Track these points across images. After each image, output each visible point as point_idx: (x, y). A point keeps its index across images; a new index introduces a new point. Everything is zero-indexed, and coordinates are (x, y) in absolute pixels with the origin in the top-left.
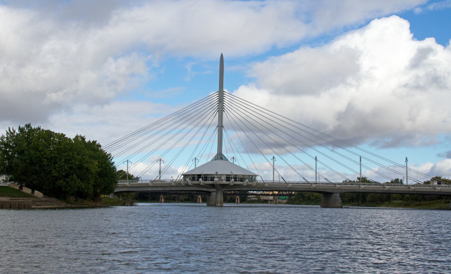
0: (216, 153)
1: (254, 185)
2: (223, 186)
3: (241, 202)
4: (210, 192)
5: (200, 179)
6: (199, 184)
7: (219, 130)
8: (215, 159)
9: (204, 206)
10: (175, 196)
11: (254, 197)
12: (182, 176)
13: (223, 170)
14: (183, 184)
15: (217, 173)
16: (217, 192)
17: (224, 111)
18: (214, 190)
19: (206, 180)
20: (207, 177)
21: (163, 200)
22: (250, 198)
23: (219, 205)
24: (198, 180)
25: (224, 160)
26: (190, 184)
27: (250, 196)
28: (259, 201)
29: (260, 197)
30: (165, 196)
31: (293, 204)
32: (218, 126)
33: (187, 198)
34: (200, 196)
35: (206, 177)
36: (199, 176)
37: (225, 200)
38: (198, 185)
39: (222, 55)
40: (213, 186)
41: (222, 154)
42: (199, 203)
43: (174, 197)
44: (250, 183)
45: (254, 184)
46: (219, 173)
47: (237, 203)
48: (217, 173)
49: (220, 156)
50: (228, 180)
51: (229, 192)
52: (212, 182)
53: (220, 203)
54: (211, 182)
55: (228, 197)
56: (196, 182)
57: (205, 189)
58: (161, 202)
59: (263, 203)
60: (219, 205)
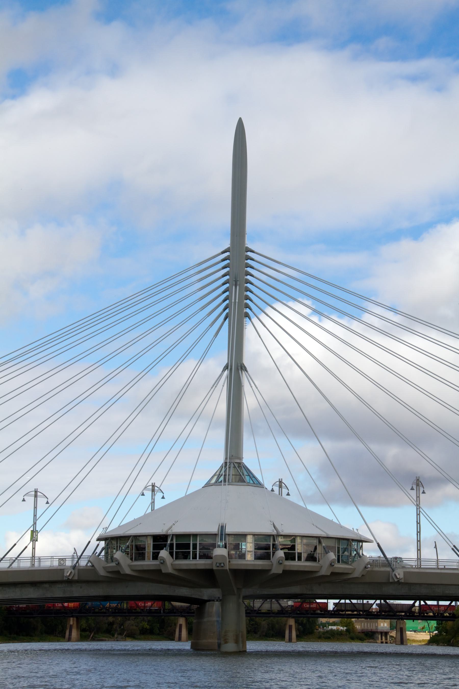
0: (221, 460)
1: (357, 574)
2: (246, 576)
3: (300, 637)
4: (202, 603)
5: (164, 553)
6: (158, 572)
7: (230, 377)
8: (217, 483)
9: (179, 653)
10: (111, 619)
11: (334, 624)
12: (102, 544)
13: (244, 517)
14: (102, 573)
15: (222, 528)
16: (222, 601)
17: (247, 315)
18: (215, 592)
19: (186, 556)
20: (188, 546)
21: (75, 633)
22: (324, 625)
23: (230, 647)
24: (155, 556)
25: (248, 484)
26: (128, 571)
27: (324, 620)
28: (351, 635)
29: (351, 623)
30: (83, 623)
31: (453, 645)
32: (226, 368)
33: (146, 626)
34: (182, 621)
35: (182, 545)
36: (160, 540)
37: (254, 632)
38: (156, 575)
39: (240, 120)
40: (209, 577)
41: (241, 465)
42: (180, 639)
43: (111, 624)
44: (340, 567)
45: (357, 570)
46: (229, 530)
47: (290, 640)
48: (222, 528)
49: (234, 471)
50: (266, 557)
51: (266, 606)
52: (208, 561)
53: (237, 642)
54: (203, 561)
55: (264, 623)
56: (148, 563)
57: (184, 592)
58: (69, 640)
59: (361, 640)
60: (230, 647)
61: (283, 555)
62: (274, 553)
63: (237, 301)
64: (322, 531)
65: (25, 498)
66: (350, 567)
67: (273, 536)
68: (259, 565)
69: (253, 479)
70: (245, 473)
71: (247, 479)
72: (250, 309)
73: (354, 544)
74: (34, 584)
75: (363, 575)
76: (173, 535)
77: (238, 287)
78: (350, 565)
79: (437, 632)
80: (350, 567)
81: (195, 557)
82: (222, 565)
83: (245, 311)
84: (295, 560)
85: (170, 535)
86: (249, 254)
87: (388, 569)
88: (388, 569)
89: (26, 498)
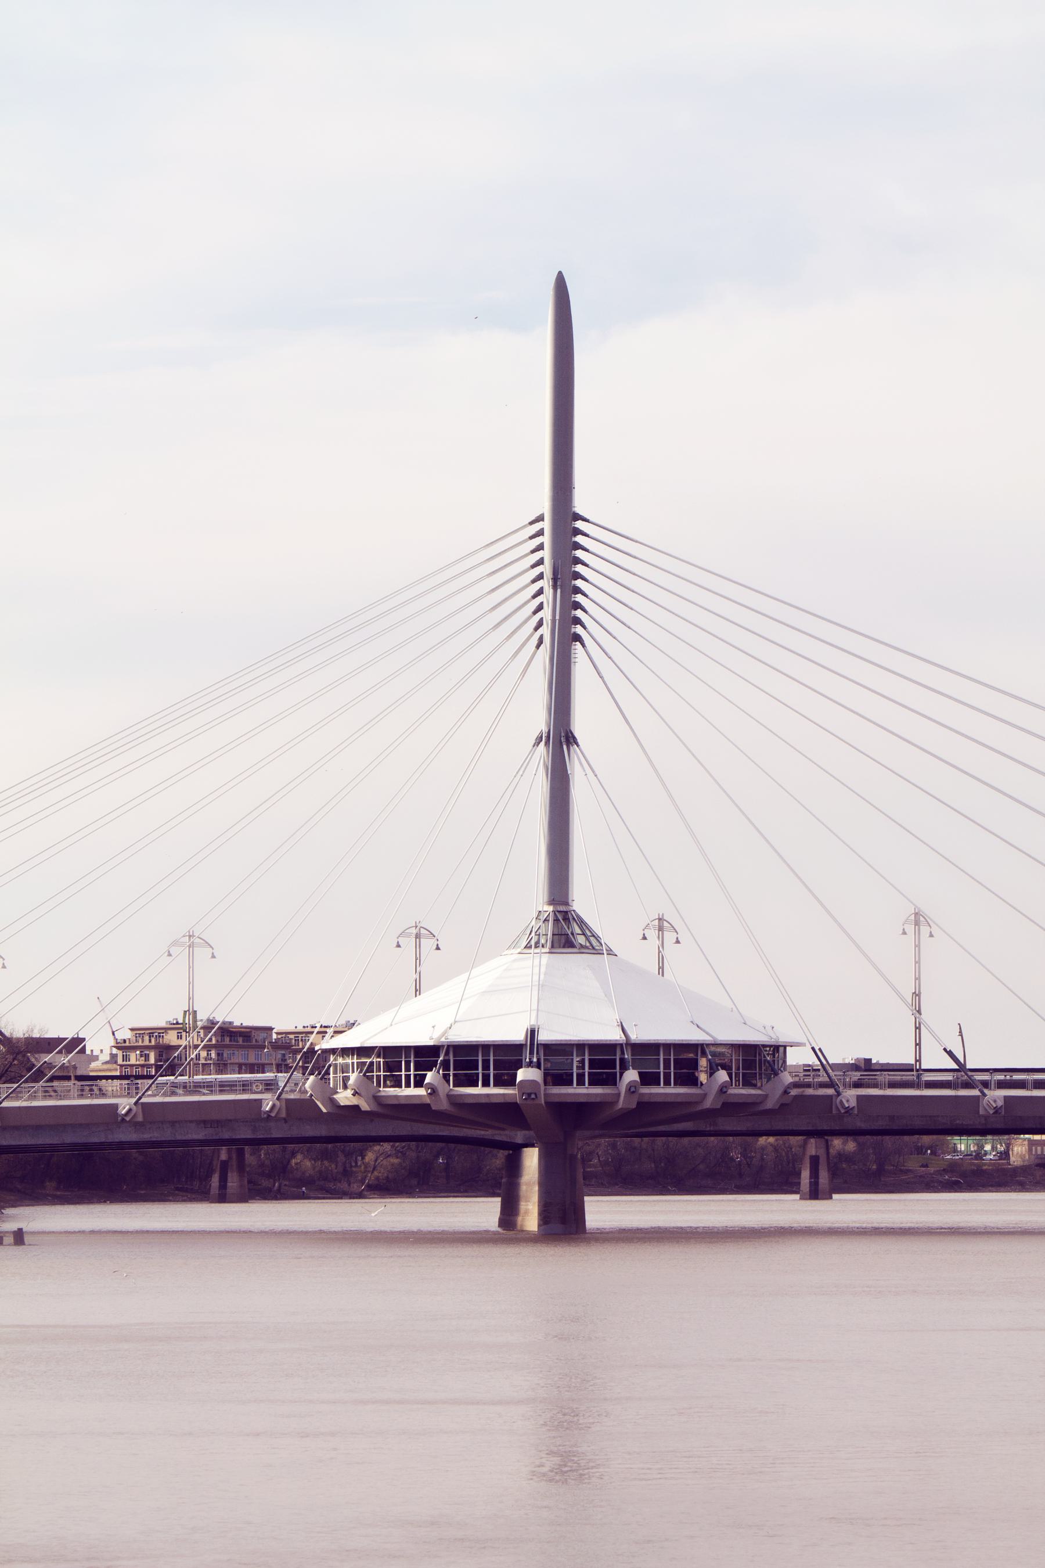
17: (577, 638)
25: (582, 949)
46: (543, 1037)
48: (532, 1033)
54: (598, 1090)
61: (637, 1078)
62: (621, 1075)
63: (557, 617)
64: (707, 1033)
65: (401, 940)
66: (759, 1092)
67: (621, 1045)
68: (597, 1095)
69: (592, 939)
70: (577, 930)
71: (581, 940)
72: (584, 627)
73: (781, 1049)
74: (38, 1128)
75: (782, 1105)
76: (448, 1046)
77: (559, 591)
78: (759, 1088)
79: (396, 1161)
80: (759, 1092)
81: (408, 1085)
82: (533, 1096)
83: (573, 630)
84: (659, 1084)
85: (443, 1046)
86: (579, 524)
87: (830, 1091)
88: (830, 1091)
89: (401, 941)
